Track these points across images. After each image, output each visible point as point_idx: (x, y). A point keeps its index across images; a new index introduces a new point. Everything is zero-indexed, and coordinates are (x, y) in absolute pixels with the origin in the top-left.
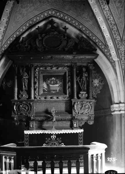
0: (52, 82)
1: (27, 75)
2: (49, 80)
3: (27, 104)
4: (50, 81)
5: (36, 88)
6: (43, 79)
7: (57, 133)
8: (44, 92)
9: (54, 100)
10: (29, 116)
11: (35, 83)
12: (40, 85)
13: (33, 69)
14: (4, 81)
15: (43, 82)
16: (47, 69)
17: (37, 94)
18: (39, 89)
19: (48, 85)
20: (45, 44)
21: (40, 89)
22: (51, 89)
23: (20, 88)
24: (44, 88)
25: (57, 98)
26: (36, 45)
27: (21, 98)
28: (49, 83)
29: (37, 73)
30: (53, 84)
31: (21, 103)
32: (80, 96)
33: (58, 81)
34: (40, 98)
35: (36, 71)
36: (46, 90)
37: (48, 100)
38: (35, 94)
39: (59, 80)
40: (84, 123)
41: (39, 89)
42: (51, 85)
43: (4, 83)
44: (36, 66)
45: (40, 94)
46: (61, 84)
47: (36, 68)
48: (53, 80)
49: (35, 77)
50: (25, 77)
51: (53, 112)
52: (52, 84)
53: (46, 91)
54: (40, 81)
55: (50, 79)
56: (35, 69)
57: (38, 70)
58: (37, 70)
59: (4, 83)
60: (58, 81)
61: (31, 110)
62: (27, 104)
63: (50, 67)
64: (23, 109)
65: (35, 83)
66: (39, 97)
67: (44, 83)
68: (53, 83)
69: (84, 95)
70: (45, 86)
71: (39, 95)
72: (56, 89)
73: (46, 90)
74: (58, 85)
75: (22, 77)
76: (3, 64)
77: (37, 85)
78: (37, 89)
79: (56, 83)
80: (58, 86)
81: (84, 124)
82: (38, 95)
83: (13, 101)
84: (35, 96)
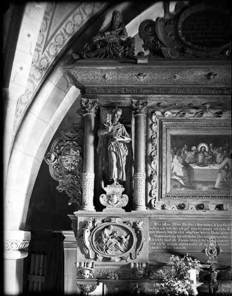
0: (200, 157)
1: (126, 133)
2: (191, 151)
3: (125, 225)
4: (193, 153)
5: (151, 175)
6: (172, 147)
7: (104, 210)
8: (175, 187)
9: (207, 212)
10: (132, 265)
11: (149, 159)
12: (164, 167)
13: (142, 116)
14: (53, 148)
15: (173, 157)
16: (187, 115)
17: (155, 193)
18: (160, 176)
19: (186, 166)
20: (183, 34)
21: (164, 179)
22: (196, 179)
23: (103, 177)
24: (175, 174)
25: (217, 207)
26: (157, 39)
27: (105, 207)
28: (189, 158)
29: (155, 127)
30: (203, 164)
31: (106, 224)
32: (103, 200)
33: (219, 155)
34: (163, 207)
35: (150, 122)
36: (181, 181)
37: (189, 212)
38: (148, 194)
39: (222, 152)
40: (102, 204)
41: (160, 176)
42: (195, 167)
43: (53, 157)
44: (152, 107)
45: (164, 192)
46: (227, 164)
47: (153, 112)
48: (203, 151)
49: (148, 141)
50: (121, 138)
51: (211, 252)
52: (199, 165)
53: (182, 186)
54: (164, 154)
55: (194, 148)
56: (149, 116)
57: (158, 117)
58: (154, 117)
59: (53, 157)
60: (219, 155)
61: (137, 247)
62: (127, 227)
63: (194, 111)
64: (114, 241)
65: (149, 159)
66: (162, 202)
67: (175, 160)
68: (203, 160)
69: (115, 198)
70: (179, 169)
71: (160, 196)
72: (214, 181)
73: (181, 181)
74: (216, 167)
75: (110, 138)
76: (49, 99)
77: (155, 165)
78: (156, 178)
79: (213, 161)
80: (220, 171)
81: (100, 202)
82: (157, 195)
83: (81, 215)
84: (149, 199)
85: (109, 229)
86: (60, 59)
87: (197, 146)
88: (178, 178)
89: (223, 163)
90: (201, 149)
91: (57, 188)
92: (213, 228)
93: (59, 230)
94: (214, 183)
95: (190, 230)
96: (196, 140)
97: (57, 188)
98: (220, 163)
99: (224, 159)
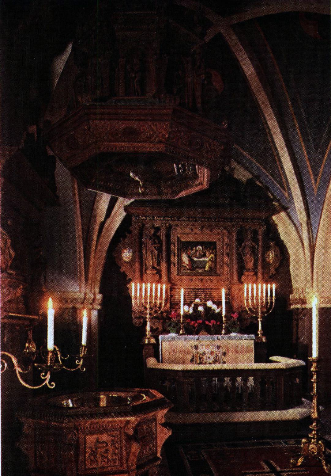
0: (198, 254)
33: (207, 253)
36: (187, 267)
46: (212, 258)
52: (197, 258)
53: (188, 269)
60: (207, 253)
73: (187, 267)
85: (204, 351)
86: (85, 287)
87: (196, 247)
88: (185, 265)
89: (210, 258)
90: (198, 249)
91: (154, 328)
92: (204, 291)
93: (149, 389)
94: (205, 268)
95: (192, 293)
96: (196, 244)
97: (154, 328)
98: (208, 257)
99: (210, 254)
